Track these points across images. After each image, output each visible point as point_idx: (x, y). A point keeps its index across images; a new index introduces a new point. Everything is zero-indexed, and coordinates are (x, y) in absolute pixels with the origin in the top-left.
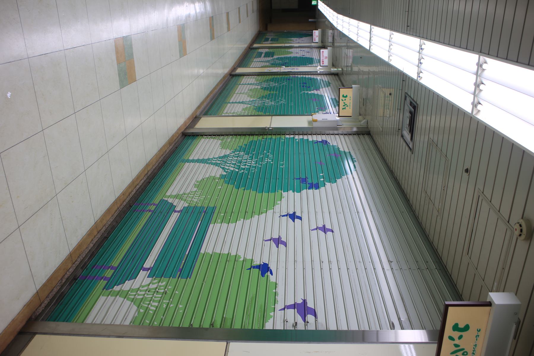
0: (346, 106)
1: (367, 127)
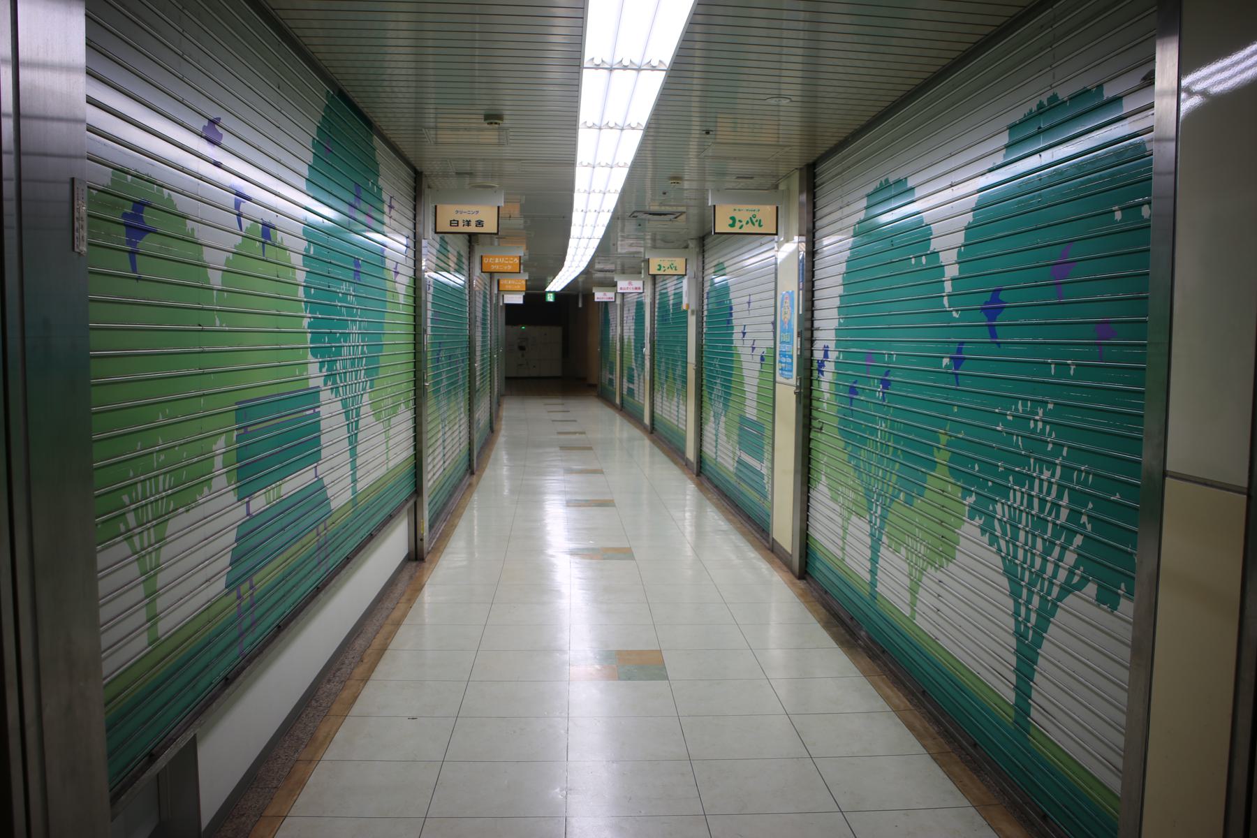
0: (754, 220)
1: (801, 169)
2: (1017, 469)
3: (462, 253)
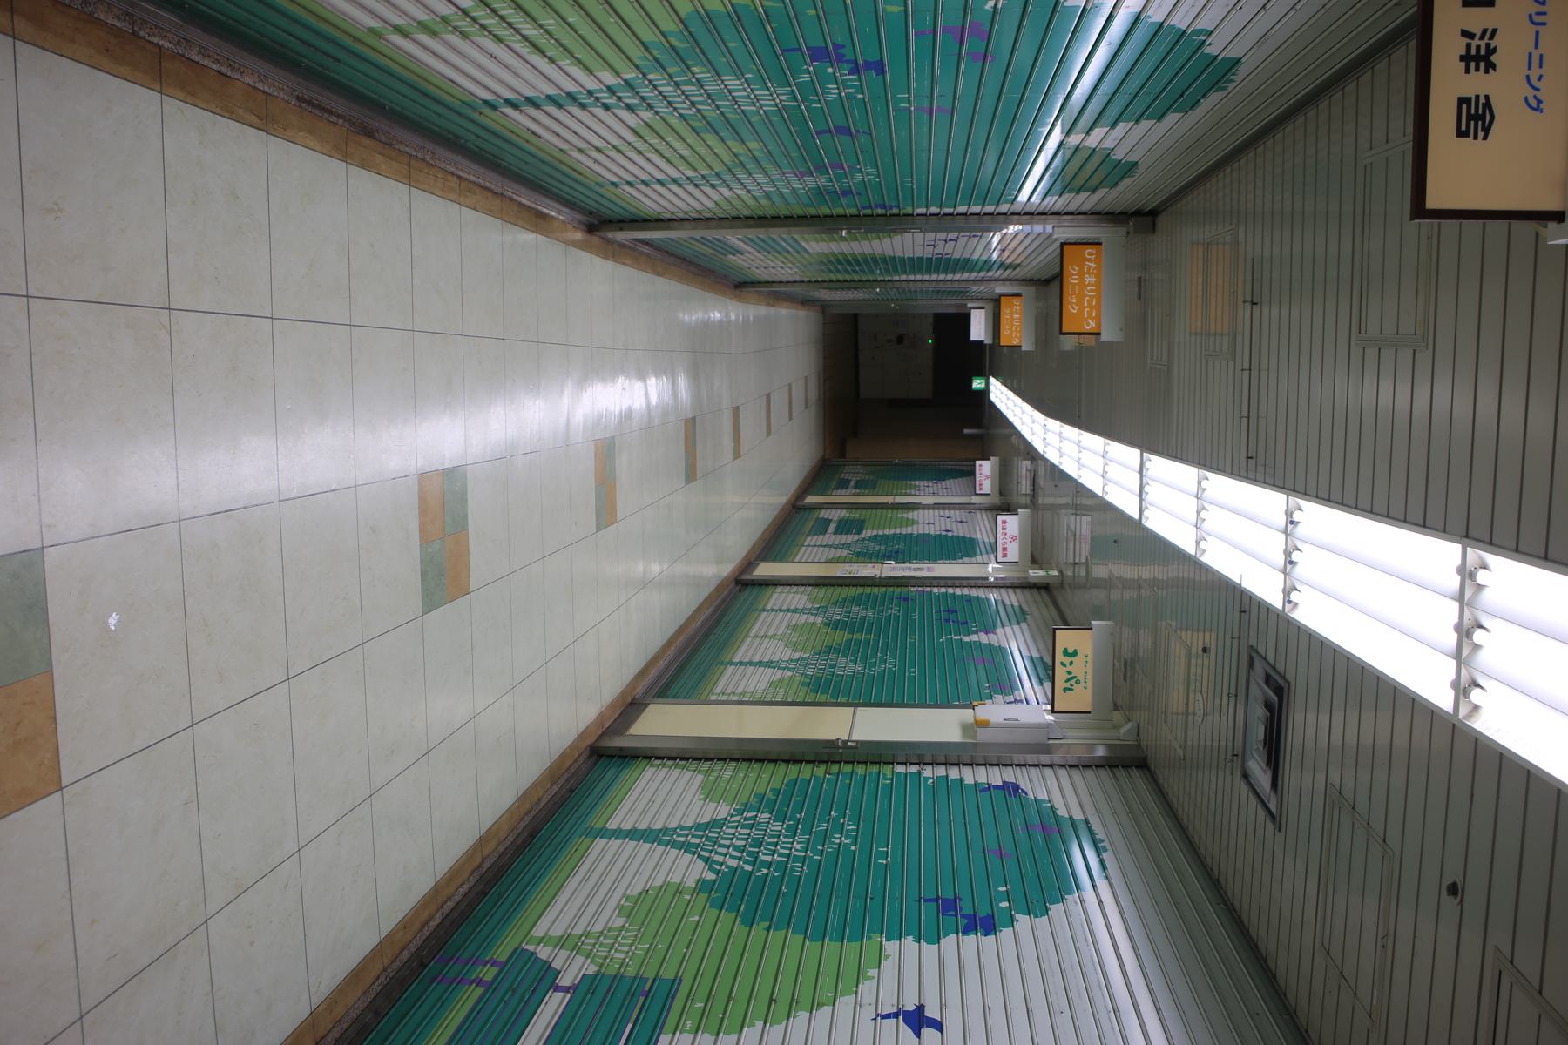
0: (1073, 682)
1: (1139, 746)
2: (800, 826)
3: (1018, 270)
